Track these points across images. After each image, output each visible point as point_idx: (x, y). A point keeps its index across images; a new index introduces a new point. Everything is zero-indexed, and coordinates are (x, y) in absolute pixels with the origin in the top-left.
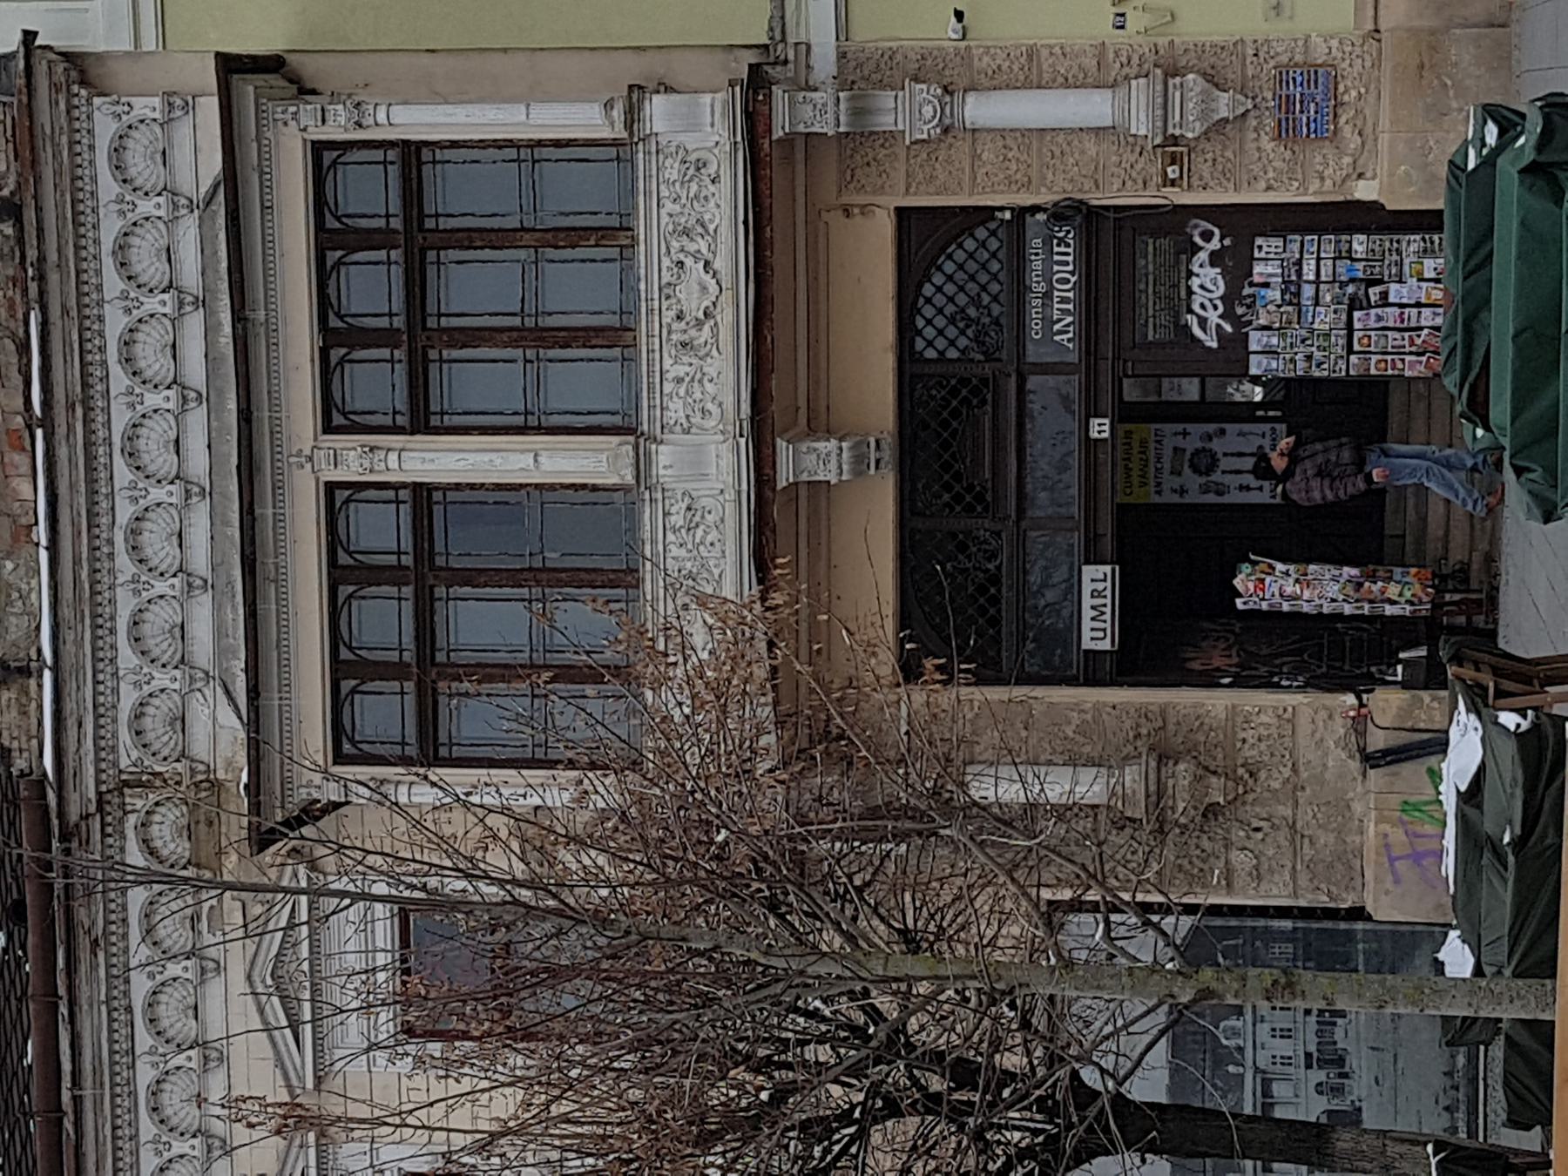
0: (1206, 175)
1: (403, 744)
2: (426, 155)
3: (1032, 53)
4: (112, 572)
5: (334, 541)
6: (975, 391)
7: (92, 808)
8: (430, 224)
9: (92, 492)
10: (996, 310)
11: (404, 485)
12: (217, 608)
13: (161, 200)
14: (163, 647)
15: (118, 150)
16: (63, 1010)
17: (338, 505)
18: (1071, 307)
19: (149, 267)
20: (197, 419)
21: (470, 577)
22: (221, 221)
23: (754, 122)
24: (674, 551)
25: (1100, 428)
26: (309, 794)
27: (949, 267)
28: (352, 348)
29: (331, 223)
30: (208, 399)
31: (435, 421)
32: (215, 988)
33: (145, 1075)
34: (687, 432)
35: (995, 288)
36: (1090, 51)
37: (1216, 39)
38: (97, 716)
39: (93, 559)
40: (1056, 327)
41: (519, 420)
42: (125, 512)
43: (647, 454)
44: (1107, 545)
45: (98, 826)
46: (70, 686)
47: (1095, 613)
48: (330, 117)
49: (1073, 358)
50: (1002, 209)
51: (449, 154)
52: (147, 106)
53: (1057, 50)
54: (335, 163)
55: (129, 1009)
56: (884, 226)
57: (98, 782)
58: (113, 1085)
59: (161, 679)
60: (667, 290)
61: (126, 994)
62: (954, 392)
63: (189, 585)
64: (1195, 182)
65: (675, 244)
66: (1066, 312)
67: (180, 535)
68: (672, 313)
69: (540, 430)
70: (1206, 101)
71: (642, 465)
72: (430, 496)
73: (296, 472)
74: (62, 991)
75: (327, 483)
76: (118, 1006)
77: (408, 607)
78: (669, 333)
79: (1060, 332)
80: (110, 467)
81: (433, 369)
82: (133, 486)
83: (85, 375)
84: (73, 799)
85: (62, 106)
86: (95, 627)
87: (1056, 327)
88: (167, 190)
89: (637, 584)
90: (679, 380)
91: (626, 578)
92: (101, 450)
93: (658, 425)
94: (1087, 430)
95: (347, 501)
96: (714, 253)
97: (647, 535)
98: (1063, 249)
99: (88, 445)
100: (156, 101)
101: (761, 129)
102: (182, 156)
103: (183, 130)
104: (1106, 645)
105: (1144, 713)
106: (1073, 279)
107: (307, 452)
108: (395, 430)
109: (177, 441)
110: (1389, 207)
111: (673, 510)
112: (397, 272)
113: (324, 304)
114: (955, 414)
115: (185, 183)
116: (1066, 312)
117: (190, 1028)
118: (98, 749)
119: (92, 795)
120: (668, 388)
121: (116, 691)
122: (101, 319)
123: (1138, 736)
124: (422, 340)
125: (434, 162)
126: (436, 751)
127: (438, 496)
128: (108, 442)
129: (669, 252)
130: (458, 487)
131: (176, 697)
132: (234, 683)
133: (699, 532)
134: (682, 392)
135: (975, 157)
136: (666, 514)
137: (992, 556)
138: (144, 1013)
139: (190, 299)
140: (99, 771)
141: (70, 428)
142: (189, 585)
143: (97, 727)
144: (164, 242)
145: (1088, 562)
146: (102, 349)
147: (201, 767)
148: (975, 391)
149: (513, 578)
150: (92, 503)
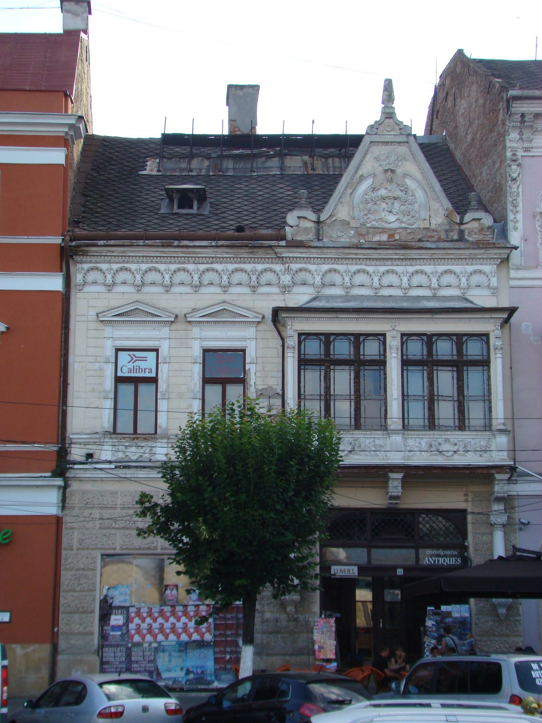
0: (479, 605)
2: (485, 368)
4: (352, 264)
7: (279, 255)
8: (465, 368)
9: (377, 259)
11: (385, 356)
12: (341, 297)
13: (466, 285)
15: (480, 272)
16: (214, 243)
17: (379, 337)
18: (437, 563)
19: (386, 280)
21: (357, 378)
23: (500, 468)
24: (368, 441)
26: (289, 325)
28: (456, 343)
32: (218, 290)
34: (404, 445)
38: (307, 258)
39: (356, 259)
40: (430, 559)
41: (405, 393)
42: (370, 269)
45: (272, 257)
46: (318, 251)
47: (343, 570)
48: (497, 340)
49: (420, 563)
52: (494, 282)
54: (482, 340)
55: (212, 263)
56: (461, 505)
57: (286, 257)
58: (188, 257)
59: (318, 279)
60: (447, 441)
61: (217, 262)
63: (348, 288)
65: (461, 443)
66: (435, 561)
67: (363, 286)
68: (441, 442)
69: (403, 400)
71: (395, 432)
72: (382, 365)
73: (390, 325)
75: (385, 334)
78: (435, 441)
79: (428, 559)
81: (421, 368)
83: (413, 259)
86: (335, 258)
87: (430, 559)
90: (420, 443)
92: (389, 263)
93: (406, 437)
94: (400, 568)
96: (459, 455)
98: (454, 560)
99: (392, 259)
100: (495, 285)
101: (498, 470)
103: (487, 292)
104: (332, 572)
106: (445, 564)
107: (396, 328)
108: (402, 355)
109: (392, 286)
111: (380, 441)
112: (449, 358)
116: (435, 561)
117: (205, 281)
119: (283, 255)
120: (418, 440)
121: (314, 264)
122: (430, 264)
124: (327, 364)
125: (483, 370)
126: (303, 365)
127: (382, 368)
128: (392, 265)
129: (459, 441)
130: (385, 374)
131: (312, 282)
132: (318, 301)
134: (417, 445)
135: (484, 534)
138: (211, 268)
139: (436, 292)
140: (290, 258)
141: (397, 254)
142: (348, 288)
143: (304, 258)
145: (359, 568)
146: (420, 265)
147: (290, 289)
149: (357, 390)
150: (373, 259)
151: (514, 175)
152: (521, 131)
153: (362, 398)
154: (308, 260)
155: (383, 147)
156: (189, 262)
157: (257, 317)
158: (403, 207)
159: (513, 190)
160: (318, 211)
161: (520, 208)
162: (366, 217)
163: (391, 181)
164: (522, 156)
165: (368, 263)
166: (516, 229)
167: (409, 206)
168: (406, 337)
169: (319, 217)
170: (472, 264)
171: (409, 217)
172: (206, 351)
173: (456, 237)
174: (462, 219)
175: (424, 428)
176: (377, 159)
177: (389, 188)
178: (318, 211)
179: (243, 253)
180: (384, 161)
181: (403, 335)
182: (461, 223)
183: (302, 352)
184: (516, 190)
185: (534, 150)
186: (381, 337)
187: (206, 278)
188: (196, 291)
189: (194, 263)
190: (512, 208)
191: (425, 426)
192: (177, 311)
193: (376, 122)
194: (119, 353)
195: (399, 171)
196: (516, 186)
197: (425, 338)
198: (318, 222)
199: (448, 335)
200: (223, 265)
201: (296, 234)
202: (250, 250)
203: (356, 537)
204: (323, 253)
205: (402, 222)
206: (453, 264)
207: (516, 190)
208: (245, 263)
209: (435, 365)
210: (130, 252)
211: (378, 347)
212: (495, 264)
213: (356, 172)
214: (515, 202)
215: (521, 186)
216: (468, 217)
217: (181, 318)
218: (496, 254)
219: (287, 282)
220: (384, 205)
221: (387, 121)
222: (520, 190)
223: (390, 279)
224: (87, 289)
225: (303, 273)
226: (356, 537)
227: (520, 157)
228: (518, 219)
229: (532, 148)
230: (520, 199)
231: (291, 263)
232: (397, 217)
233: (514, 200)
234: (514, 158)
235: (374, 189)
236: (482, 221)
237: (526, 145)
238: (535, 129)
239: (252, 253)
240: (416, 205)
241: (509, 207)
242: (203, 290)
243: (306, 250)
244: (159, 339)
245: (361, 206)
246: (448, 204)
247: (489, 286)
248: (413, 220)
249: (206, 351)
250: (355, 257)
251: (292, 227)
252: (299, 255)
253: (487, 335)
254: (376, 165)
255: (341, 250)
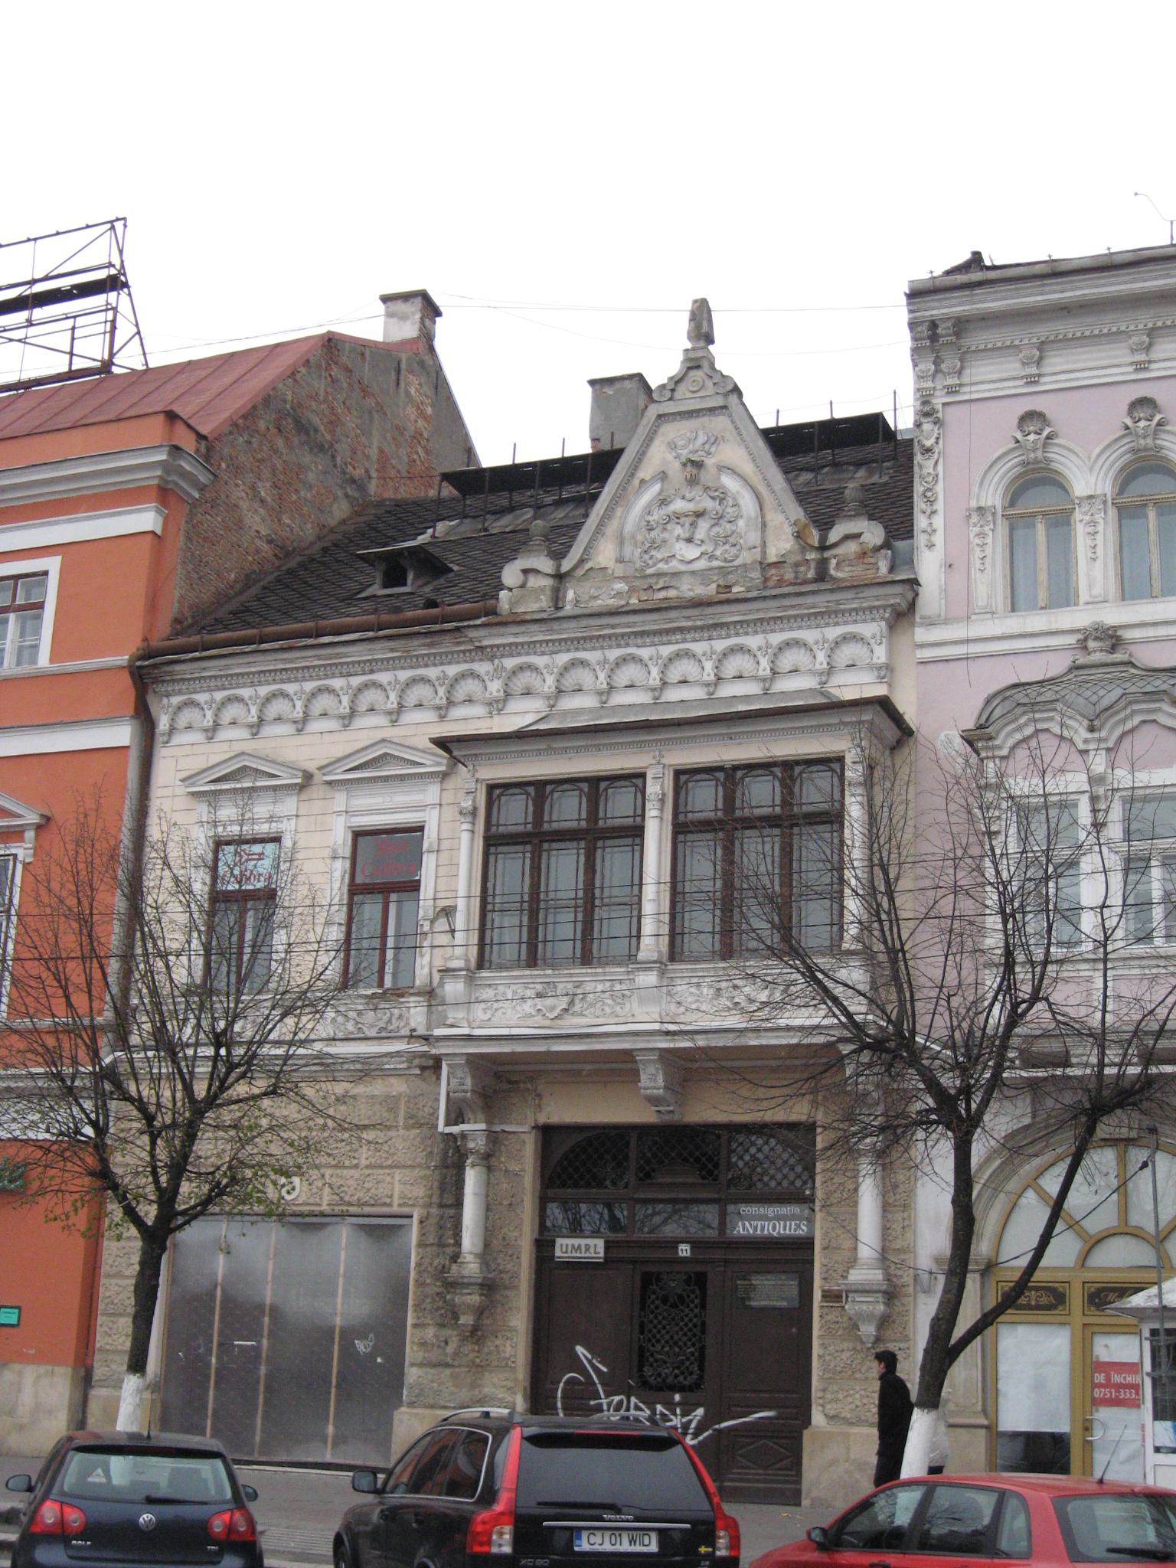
0: (829, 1317)
1: (551, 821)
2: (638, 840)
3: (906, 1207)
4: (610, 647)
5: (614, 779)
6: (710, 1173)
10: (759, 1185)
12: (591, 710)
14: (569, 682)
19: (788, 660)
20: (698, 693)
22: (811, 702)
25: (684, 1250)
27: (785, 1156)
28: (724, 785)
29: (739, 774)
30: (711, 699)
31: (681, 838)
33: (337, 683)
35: (785, 1183)
36: (905, 1244)
37: (911, 1324)
39: (616, 636)
42: (645, 653)
43: (650, 969)
44: (615, 1254)
46: (544, 627)
50: (813, 1188)
51: (637, 855)
53: (906, 1223)
57: (492, 646)
59: (550, 680)
61: (380, 670)
62: (710, 1159)
64: (826, 1310)
70: (868, 1317)
71: (646, 966)
74: (381, 633)
76: (371, 666)
77: (574, 825)
80: (669, 643)
82: (659, 657)
84: (482, 632)
85: (877, 603)
86: (578, 639)
88: (611, 688)
89: (724, 959)
91: (587, 959)
95: (636, 786)
97: (607, 970)
102: (851, 677)
104: (558, 1253)
105: (516, 1275)
107: (663, 761)
110: (805, 1432)
113: (751, 767)
114: (697, 1160)
115: (837, 679)
118: (510, 645)
121: (543, 654)
123: (501, 1272)
124: (536, 841)
128: (684, 641)
133: (609, 1002)
136: (621, 981)
137: (614, 1184)
140: (498, 646)
144: (802, 669)
145: (606, 1242)
148: (710, 1173)
151: (928, 443)
152: (937, 357)
153: (597, 902)
154: (531, 647)
155: (685, 422)
156: (333, 676)
157: (295, 777)
158: (716, 529)
159: (925, 471)
160: (558, 556)
161: (939, 505)
162: (646, 557)
163: (692, 482)
164: (944, 404)
165: (639, 641)
166: (931, 546)
167: (728, 526)
168: (683, 776)
169: (559, 566)
170: (837, 624)
171: (727, 547)
172: (358, 835)
173: (811, 574)
174: (823, 538)
175: (713, 956)
176: (672, 446)
177: (688, 496)
178: (558, 556)
179: (421, 649)
180: (684, 447)
181: (678, 773)
182: (823, 547)
183: (494, 821)
184: (931, 470)
185: (1153, 366)
186: (637, 778)
187: (729, 667)
188: (346, 726)
189: (342, 675)
190: (923, 506)
191: (714, 952)
192: (311, 767)
193: (671, 379)
194: (360, 839)
195: (710, 462)
196: (931, 462)
197: (531, 790)
198: (560, 577)
199: (766, 766)
200: (441, 668)
201: (517, 602)
202: (428, 640)
203: (608, 1182)
204: (551, 631)
205: (712, 557)
206: (800, 628)
207: (931, 470)
208: (426, 666)
209: (600, 838)
210: (237, 666)
211: (632, 800)
212: (883, 618)
213: (633, 475)
214: (929, 494)
215: (941, 461)
216: (834, 536)
217: (319, 778)
218: (877, 598)
219: (495, 694)
220: (678, 530)
221: (693, 373)
222: (940, 468)
223: (684, 668)
224: (177, 739)
225: (528, 673)
226: (608, 1182)
227: (940, 407)
228: (935, 526)
229: (1150, 362)
230: (939, 488)
231: (503, 656)
232: (703, 548)
233: (929, 490)
234: (927, 408)
235: (663, 502)
236: (862, 539)
237: (950, 381)
238: (964, 349)
239: (431, 645)
240: (741, 523)
241: (919, 504)
242: (359, 722)
243: (522, 629)
244: (422, 807)
245: (639, 538)
246: (797, 513)
247: (611, 688)
248: (734, 551)
249: (358, 835)
250: (611, 631)
251: (510, 590)
252: (511, 640)
253: (840, 759)
254: (670, 457)
255: (585, 622)
